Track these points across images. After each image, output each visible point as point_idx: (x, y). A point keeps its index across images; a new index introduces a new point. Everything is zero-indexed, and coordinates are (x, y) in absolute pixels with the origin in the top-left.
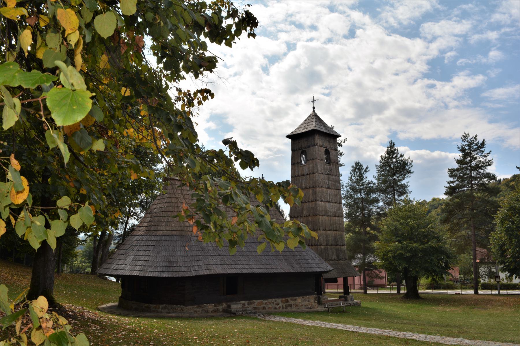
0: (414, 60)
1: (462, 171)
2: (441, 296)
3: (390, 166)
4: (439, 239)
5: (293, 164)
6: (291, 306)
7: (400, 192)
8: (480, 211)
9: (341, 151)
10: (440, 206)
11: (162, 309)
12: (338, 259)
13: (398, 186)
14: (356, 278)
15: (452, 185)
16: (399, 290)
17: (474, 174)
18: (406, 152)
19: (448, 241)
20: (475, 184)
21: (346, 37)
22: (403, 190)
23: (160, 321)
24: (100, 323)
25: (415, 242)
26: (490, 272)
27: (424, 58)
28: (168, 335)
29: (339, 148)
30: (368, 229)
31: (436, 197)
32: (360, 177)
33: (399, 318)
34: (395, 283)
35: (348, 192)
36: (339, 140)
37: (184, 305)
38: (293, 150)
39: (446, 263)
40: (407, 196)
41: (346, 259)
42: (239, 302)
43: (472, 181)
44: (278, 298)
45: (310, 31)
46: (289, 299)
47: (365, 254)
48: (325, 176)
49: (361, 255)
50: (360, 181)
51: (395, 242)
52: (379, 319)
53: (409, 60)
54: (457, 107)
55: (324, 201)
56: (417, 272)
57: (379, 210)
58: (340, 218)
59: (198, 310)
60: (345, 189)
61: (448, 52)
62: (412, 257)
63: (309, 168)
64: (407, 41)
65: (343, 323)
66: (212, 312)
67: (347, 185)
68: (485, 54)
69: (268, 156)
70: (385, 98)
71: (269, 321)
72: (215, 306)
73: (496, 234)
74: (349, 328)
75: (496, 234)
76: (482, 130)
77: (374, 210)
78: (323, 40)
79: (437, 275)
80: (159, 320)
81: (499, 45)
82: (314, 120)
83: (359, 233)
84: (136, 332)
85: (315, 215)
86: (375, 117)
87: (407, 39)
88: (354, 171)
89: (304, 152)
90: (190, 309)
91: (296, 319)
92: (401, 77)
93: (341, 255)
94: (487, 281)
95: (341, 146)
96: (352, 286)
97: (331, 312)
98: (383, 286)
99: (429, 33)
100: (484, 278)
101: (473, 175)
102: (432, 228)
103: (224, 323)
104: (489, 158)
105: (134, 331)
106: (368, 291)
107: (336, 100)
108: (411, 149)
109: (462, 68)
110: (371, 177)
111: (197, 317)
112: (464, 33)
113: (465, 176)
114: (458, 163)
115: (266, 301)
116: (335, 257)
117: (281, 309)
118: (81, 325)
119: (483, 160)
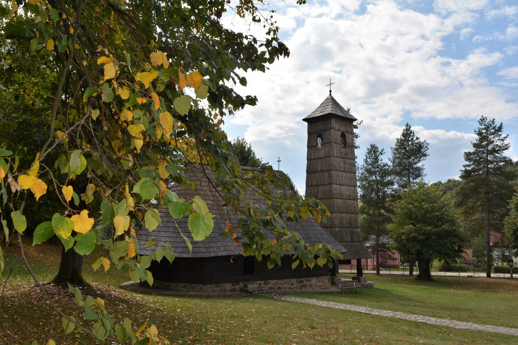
0: (428, 36)
1: (478, 155)
2: (453, 278)
3: (405, 148)
4: (452, 222)
5: (309, 147)
6: (305, 286)
7: (415, 175)
8: (495, 195)
9: (357, 133)
10: (455, 188)
11: (182, 287)
12: (352, 241)
13: (413, 168)
14: (369, 260)
15: (468, 168)
16: (411, 271)
17: (490, 158)
18: (422, 134)
19: (462, 224)
20: (490, 168)
21: (357, 13)
22: (418, 173)
23: (182, 300)
24: (126, 302)
25: (429, 225)
26: (503, 255)
27: (439, 34)
28: (190, 315)
29: (355, 130)
30: (382, 211)
31: (452, 178)
32: (375, 159)
33: (411, 300)
34: (408, 264)
35: (363, 174)
36: (355, 123)
37: (203, 284)
38: (309, 133)
39: (460, 247)
40: (422, 179)
41: (360, 242)
42: (255, 282)
43: (488, 165)
44: (293, 278)
45: (320, 6)
46: (303, 279)
47: (378, 236)
48: (341, 159)
49: (375, 236)
50: (375, 163)
51: (409, 225)
52: (391, 301)
53: (423, 37)
54: (472, 86)
55: (340, 185)
56: (430, 255)
57: (393, 193)
58: (355, 201)
59: (216, 289)
60: (360, 171)
61: (463, 28)
62: (425, 239)
63: (325, 152)
64: (421, 17)
65: (356, 304)
66: (230, 291)
67: (362, 167)
68: (503, 30)
69: (280, 134)
70: (398, 76)
71: (284, 301)
72: (233, 285)
73: (511, 219)
74: (362, 309)
75: (511, 219)
76: (498, 111)
77: (389, 192)
78: (333, 15)
79: (449, 258)
80: (180, 299)
81: (516, 21)
82: (331, 103)
83: (373, 215)
84: (161, 311)
85: (330, 198)
86: (387, 96)
87: (420, 14)
88: (369, 153)
89: (320, 136)
90: (208, 288)
91: (311, 300)
92: (414, 54)
93: (355, 238)
94: (500, 264)
95: (357, 128)
96: (365, 267)
97: (345, 293)
98: (396, 267)
99: (443, 9)
100: (497, 262)
101: (489, 159)
102: (446, 211)
103: (242, 302)
104: (506, 142)
105: (158, 310)
106: (381, 272)
107: (347, 77)
108: (426, 129)
109: (477, 45)
110: (386, 159)
111: (216, 296)
112: (480, 8)
113: (481, 160)
114: (474, 147)
115: (282, 281)
116: (349, 239)
117: (296, 289)
118: (110, 304)
119: (499, 144)
